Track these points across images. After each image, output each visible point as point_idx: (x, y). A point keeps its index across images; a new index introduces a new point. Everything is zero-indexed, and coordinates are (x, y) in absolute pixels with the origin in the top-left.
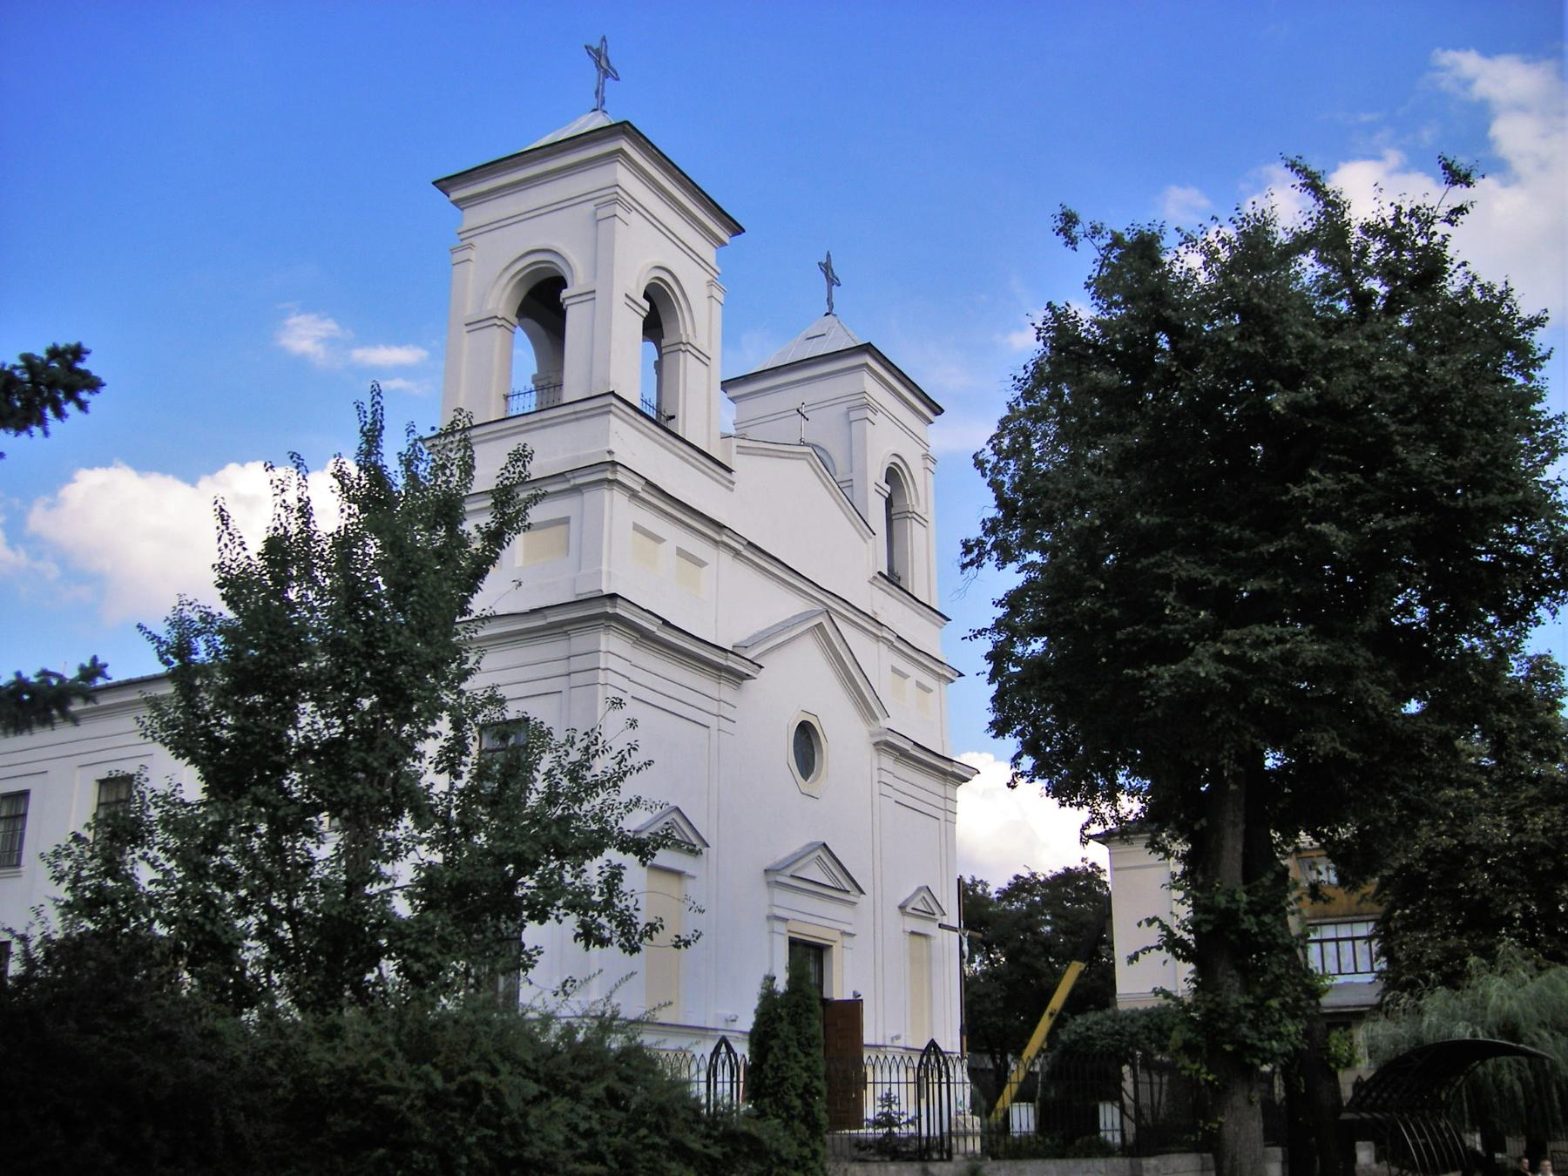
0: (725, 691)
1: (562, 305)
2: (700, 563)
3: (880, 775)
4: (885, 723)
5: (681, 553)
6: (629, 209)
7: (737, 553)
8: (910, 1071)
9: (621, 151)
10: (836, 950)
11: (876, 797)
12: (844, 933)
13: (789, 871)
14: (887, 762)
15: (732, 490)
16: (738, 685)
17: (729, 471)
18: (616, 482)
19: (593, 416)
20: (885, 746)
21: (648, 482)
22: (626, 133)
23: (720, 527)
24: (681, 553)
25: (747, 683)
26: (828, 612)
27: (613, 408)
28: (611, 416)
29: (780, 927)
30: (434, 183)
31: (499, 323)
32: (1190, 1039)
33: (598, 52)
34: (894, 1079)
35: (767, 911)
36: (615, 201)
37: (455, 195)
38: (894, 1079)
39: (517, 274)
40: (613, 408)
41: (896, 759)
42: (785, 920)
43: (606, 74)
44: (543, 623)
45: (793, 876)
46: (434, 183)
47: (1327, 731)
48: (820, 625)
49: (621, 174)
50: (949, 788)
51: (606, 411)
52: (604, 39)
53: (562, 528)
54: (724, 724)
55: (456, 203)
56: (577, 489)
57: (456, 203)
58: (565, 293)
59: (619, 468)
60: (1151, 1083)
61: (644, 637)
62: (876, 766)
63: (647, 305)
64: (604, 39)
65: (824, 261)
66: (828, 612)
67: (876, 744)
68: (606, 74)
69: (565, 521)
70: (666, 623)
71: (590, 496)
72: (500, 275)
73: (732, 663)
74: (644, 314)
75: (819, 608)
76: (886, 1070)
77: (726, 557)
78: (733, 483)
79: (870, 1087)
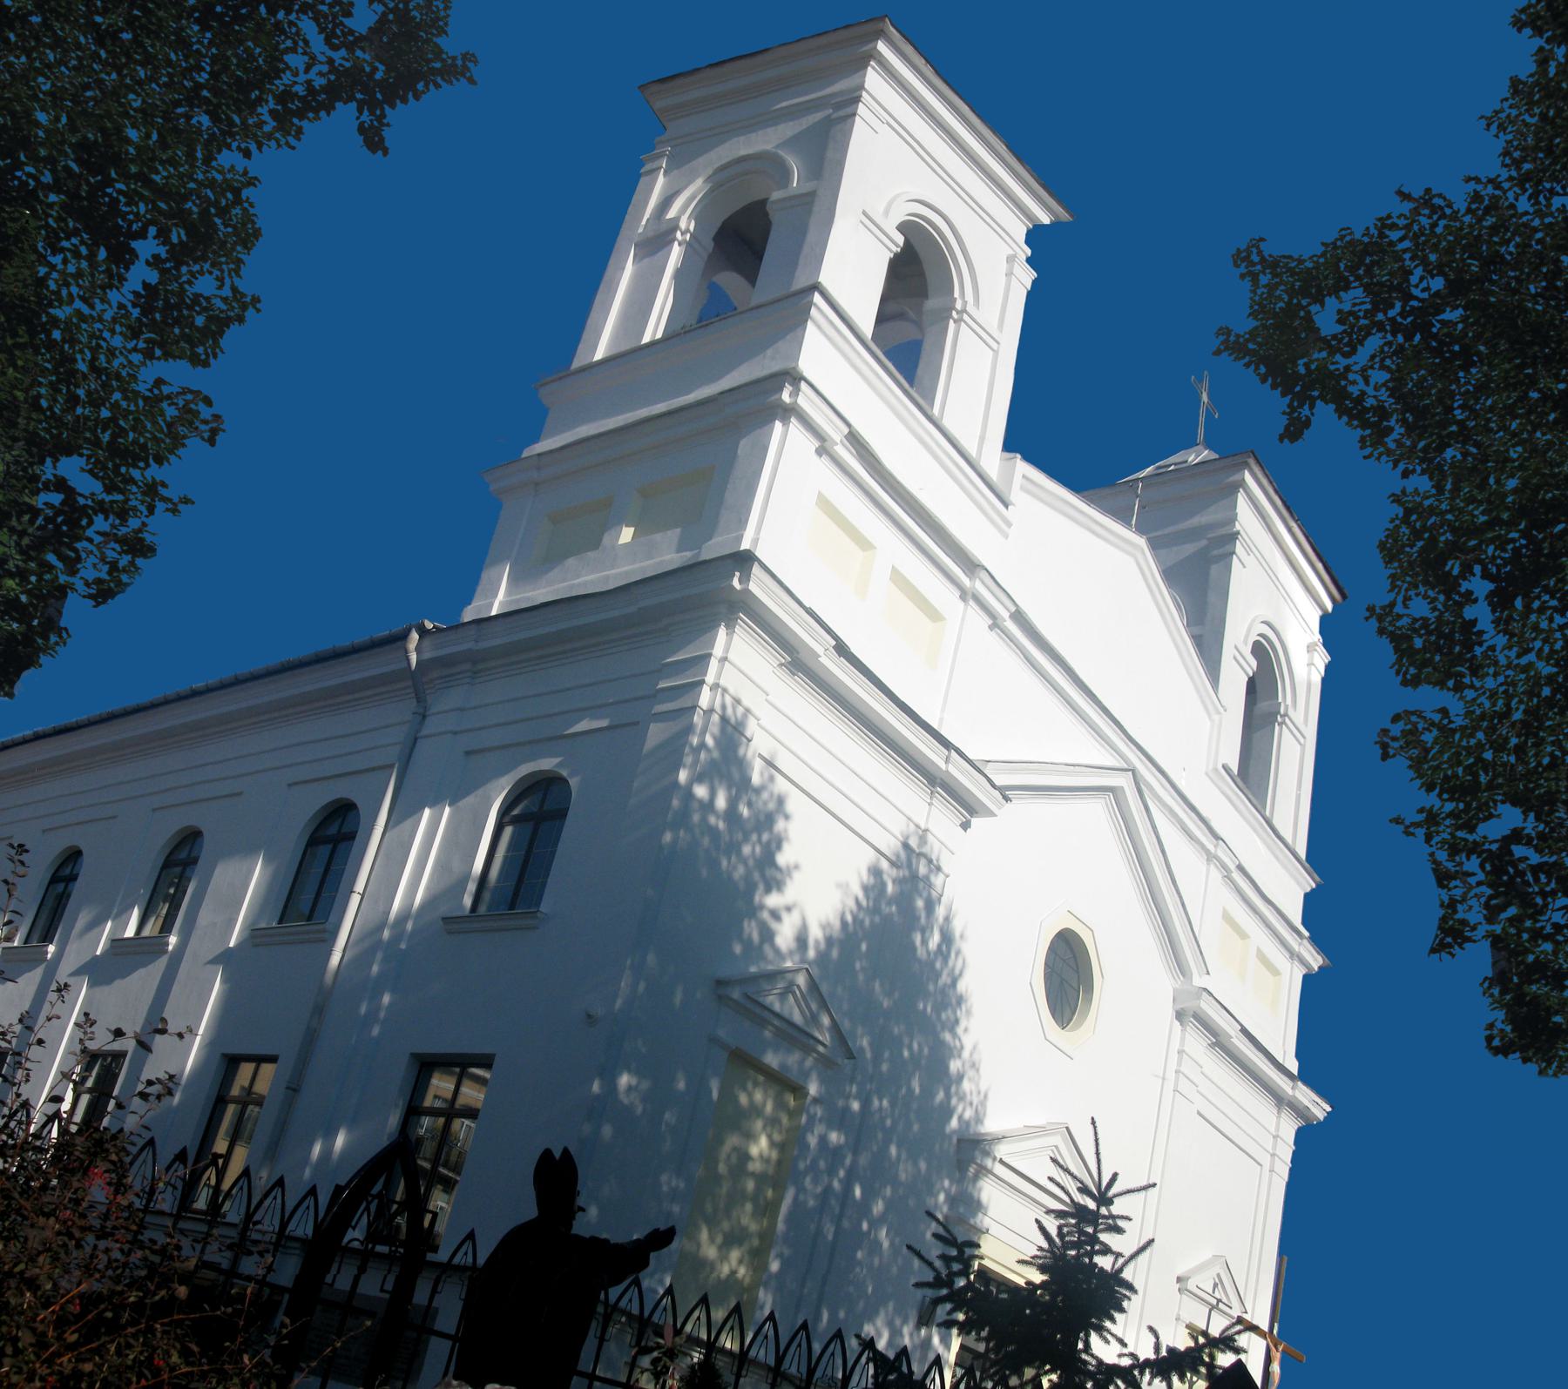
4: (1199, 981)
5: (898, 578)
14: (1197, 1043)
15: (1006, 536)
23: (971, 565)
24: (898, 578)
70: (842, 649)
78: (1009, 525)
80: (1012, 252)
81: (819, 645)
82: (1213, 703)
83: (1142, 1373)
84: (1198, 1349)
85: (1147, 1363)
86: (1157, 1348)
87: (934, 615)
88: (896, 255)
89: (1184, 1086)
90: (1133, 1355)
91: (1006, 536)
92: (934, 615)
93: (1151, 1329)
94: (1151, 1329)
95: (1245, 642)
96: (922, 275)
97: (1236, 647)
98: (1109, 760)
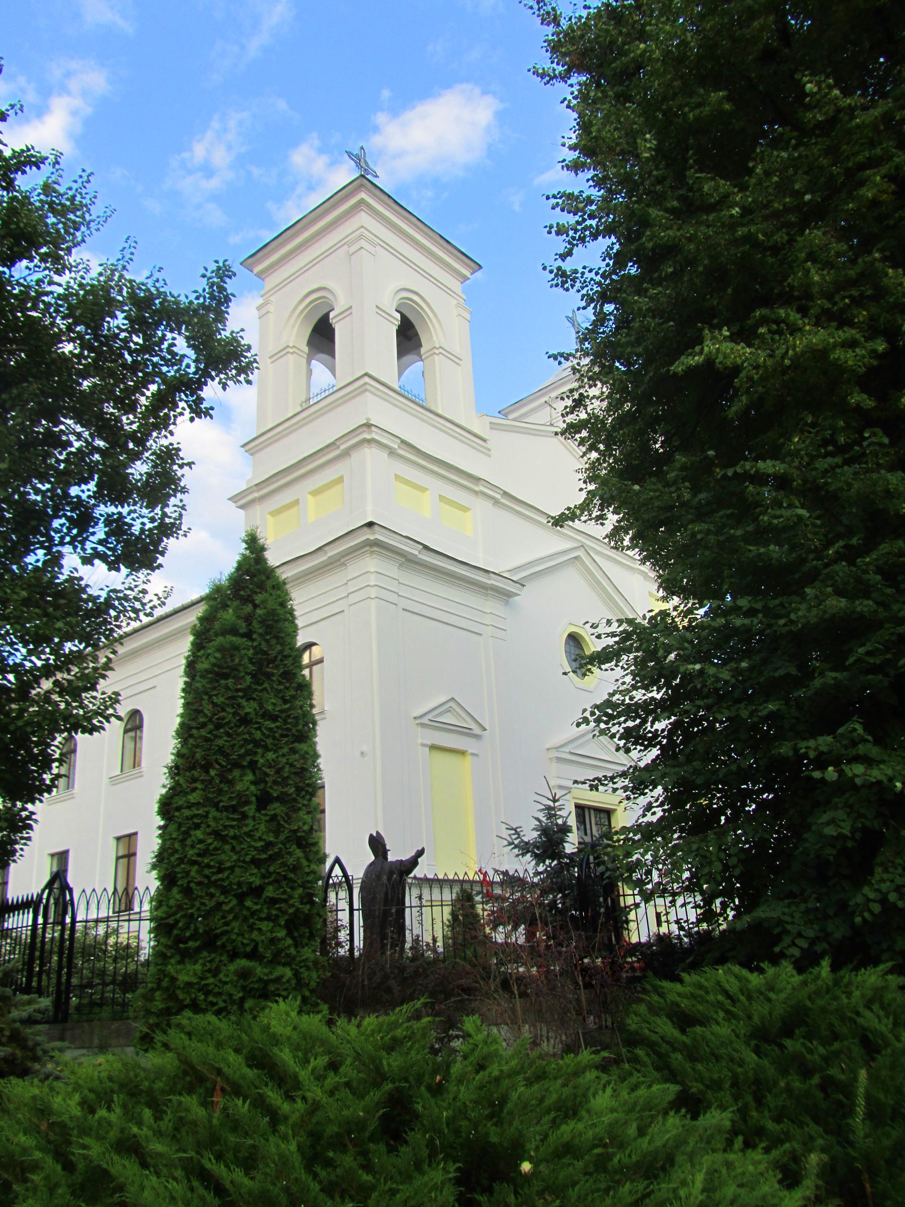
2: (464, 509)
7: (496, 502)
9: (362, 202)
13: (567, 749)
18: (373, 440)
19: (354, 397)
20: (224, 272)
21: (403, 442)
23: (477, 480)
27: (368, 387)
28: (368, 393)
33: (357, 156)
36: (361, 237)
37: (257, 269)
38: (437, 910)
39: (302, 312)
40: (368, 387)
44: (325, 558)
47: (801, 1125)
51: (363, 390)
53: (339, 487)
55: (259, 275)
56: (346, 453)
57: (259, 275)
59: (373, 429)
60: (513, 1009)
61: (408, 561)
69: (340, 480)
70: (426, 547)
71: (355, 456)
72: (290, 317)
76: (93, 906)
81: (414, 550)
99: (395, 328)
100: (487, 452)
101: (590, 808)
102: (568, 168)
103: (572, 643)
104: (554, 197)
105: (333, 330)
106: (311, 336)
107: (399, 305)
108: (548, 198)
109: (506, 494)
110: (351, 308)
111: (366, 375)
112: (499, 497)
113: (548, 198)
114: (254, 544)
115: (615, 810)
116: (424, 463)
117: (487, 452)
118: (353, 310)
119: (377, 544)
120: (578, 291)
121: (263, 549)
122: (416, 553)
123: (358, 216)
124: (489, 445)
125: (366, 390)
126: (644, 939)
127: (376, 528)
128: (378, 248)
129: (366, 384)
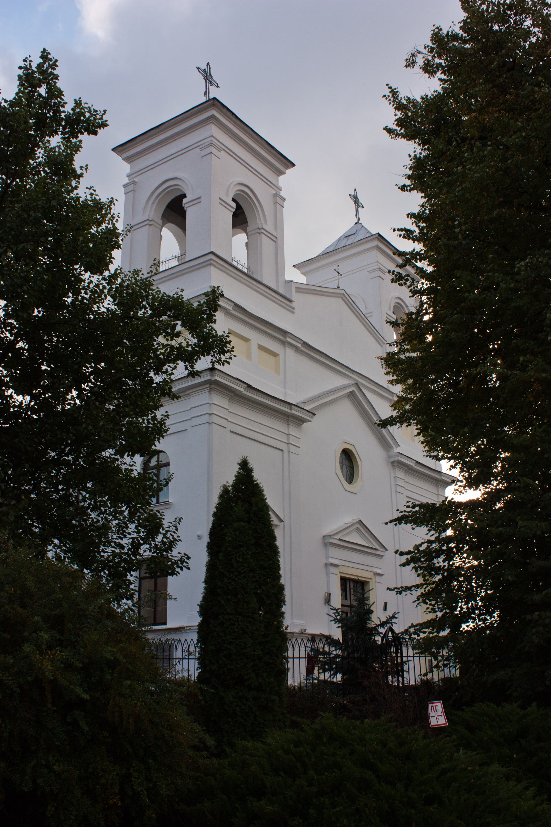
0: (293, 430)
1: (183, 208)
3: (395, 481)
4: (397, 450)
5: (261, 347)
6: (219, 150)
8: (302, 649)
9: (213, 117)
10: (371, 585)
11: (394, 493)
12: (376, 574)
13: (338, 537)
14: (400, 474)
15: (293, 313)
16: (300, 425)
17: (291, 301)
19: (200, 268)
22: (214, 105)
23: (285, 333)
24: (261, 347)
25: (305, 425)
26: (357, 384)
27: (212, 262)
29: (332, 569)
30: (113, 150)
31: (151, 223)
32: (394, 354)
34: (296, 655)
35: (324, 561)
36: (211, 144)
38: (296, 655)
41: (406, 472)
42: (336, 566)
43: (211, 84)
45: (340, 540)
46: (113, 150)
48: (352, 393)
49: (213, 130)
50: (440, 489)
51: (209, 264)
52: (208, 64)
54: (292, 448)
58: (185, 201)
62: (393, 476)
63: (234, 205)
64: (208, 64)
65: (353, 194)
66: (357, 384)
67: (393, 463)
68: (211, 84)
70: (249, 386)
73: (296, 412)
74: (233, 210)
75: (352, 382)
76: (296, 648)
77: (290, 352)
78: (294, 308)
79: (290, 660)
80: (274, 192)
81: (241, 389)
82: (381, 340)
83: (378, 627)
84: (388, 619)
85: (379, 625)
86: (380, 621)
87: (275, 355)
88: (234, 213)
89: (399, 489)
90: (375, 624)
91: (293, 313)
92: (275, 355)
93: (379, 618)
94: (379, 618)
95: (389, 309)
96: (244, 213)
97: (387, 314)
98: (346, 382)
99: (231, 214)
100: (292, 310)
101: (350, 580)
102: (399, 188)
103: (344, 456)
104: (398, 230)
105: (185, 212)
106: (165, 210)
107: (235, 195)
108: (394, 230)
109: (305, 344)
110: (200, 197)
111: (212, 253)
112: (299, 345)
113: (394, 230)
114: (244, 465)
115: (368, 582)
116: (246, 319)
117: (292, 310)
118: (201, 200)
119: (216, 383)
120: (409, 287)
121: (251, 470)
122: (242, 390)
123: (208, 127)
124: (294, 305)
125: (211, 264)
126: (412, 682)
127: (217, 372)
128: (223, 152)
129: (211, 259)
